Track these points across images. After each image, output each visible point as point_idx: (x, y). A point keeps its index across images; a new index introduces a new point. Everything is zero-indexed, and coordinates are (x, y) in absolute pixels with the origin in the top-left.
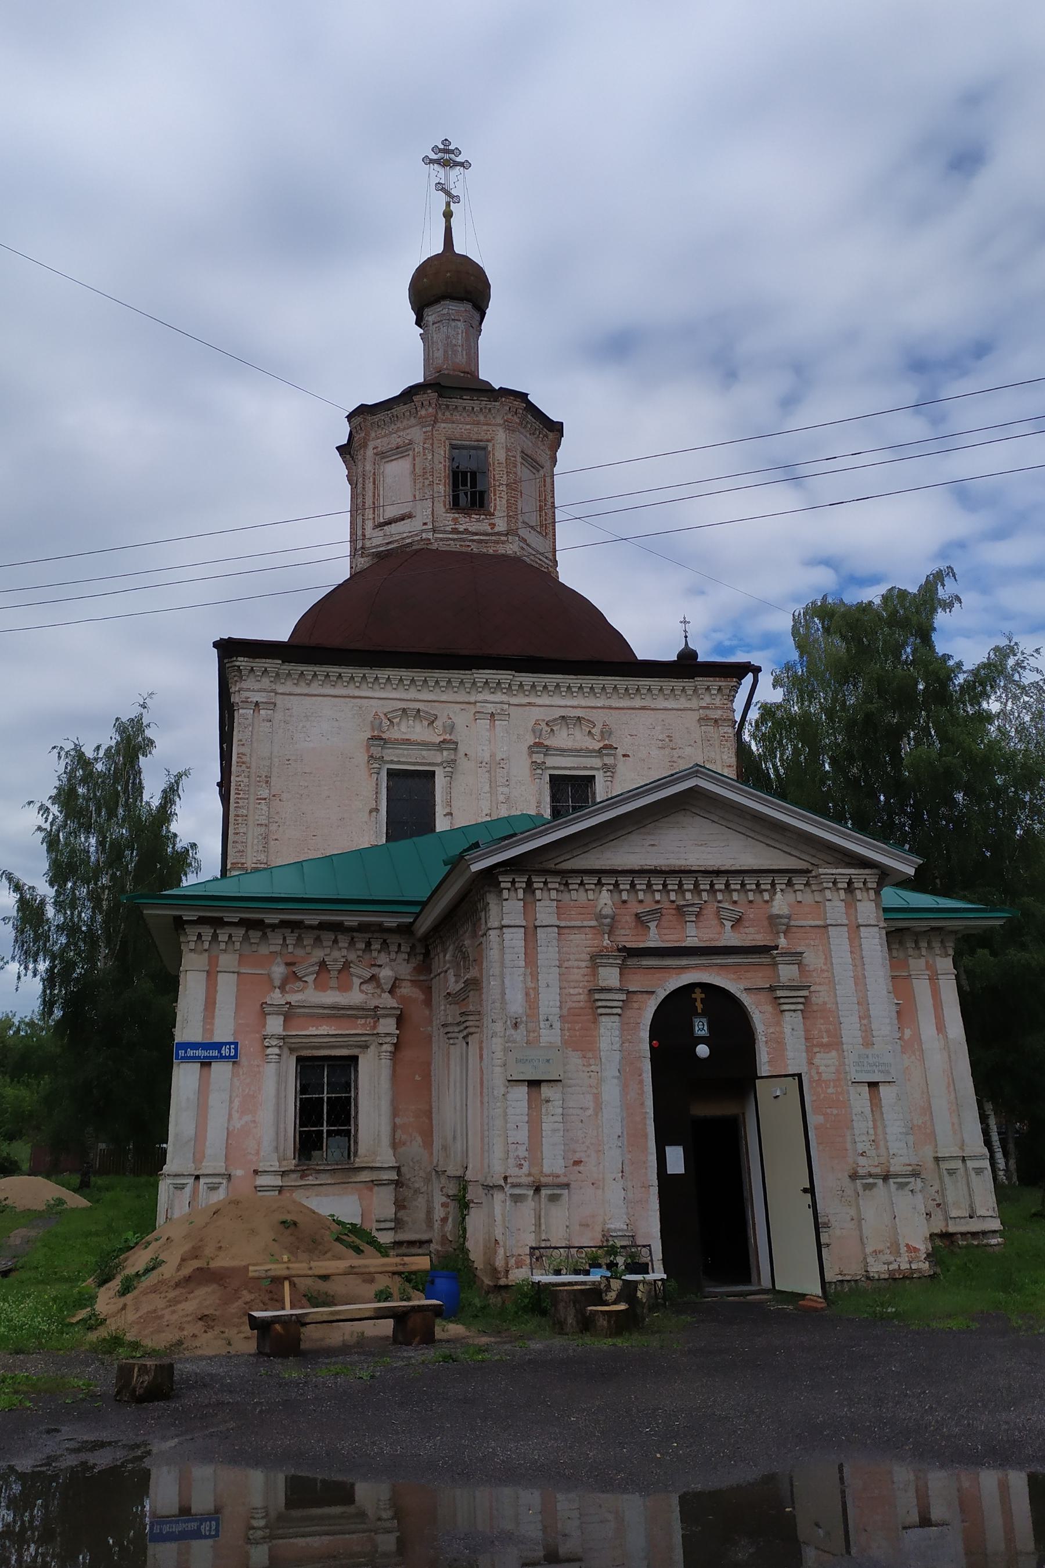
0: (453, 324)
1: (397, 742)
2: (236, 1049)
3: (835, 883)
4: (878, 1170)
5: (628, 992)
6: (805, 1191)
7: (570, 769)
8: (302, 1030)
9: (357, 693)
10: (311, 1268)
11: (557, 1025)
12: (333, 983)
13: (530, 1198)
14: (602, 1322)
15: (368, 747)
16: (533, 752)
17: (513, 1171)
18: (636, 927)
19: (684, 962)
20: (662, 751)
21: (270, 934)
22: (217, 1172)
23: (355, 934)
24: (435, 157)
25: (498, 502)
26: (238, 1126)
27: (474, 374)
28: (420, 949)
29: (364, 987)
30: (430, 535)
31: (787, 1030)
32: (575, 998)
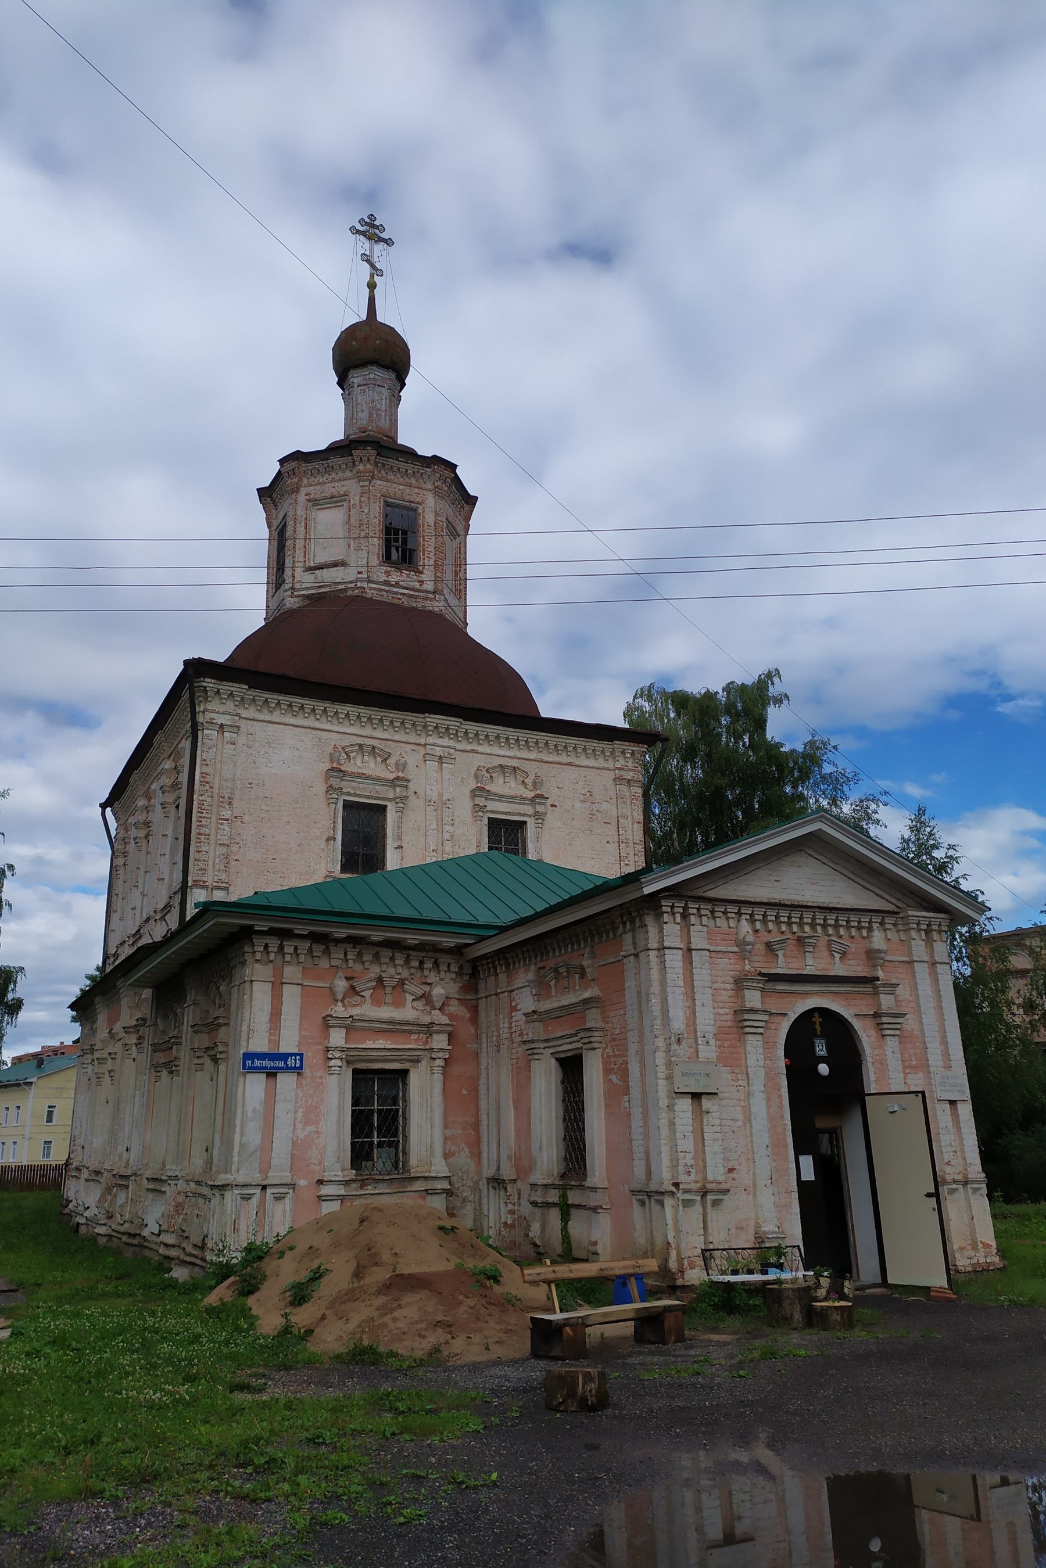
0: (378, 389)
1: (352, 775)
2: (301, 1060)
3: (918, 924)
4: (960, 1177)
5: (771, 1014)
6: (929, 1195)
7: (506, 814)
8: (362, 1043)
9: (317, 725)
10: (571, 1271)
11: (712, 1042)
12: (389, 999)
13: (698, 1203)
14: (836, 1317)
15: (327, 778)
16: (475, 796)
17: (682, 1178)
18: (766, 955)
19: (808, 988)
20: (584, 805)
21: (332, 948)
22: (283, 1182)
23: (411, 952)
24: (361, 229)
25: (427, 559)
26: (302, 1136)
27: (394, 439)
28: (467, 970)
29: (415, 1004)
30: (365, 585)
31: (889, 1053)
32: (724, 1018)
